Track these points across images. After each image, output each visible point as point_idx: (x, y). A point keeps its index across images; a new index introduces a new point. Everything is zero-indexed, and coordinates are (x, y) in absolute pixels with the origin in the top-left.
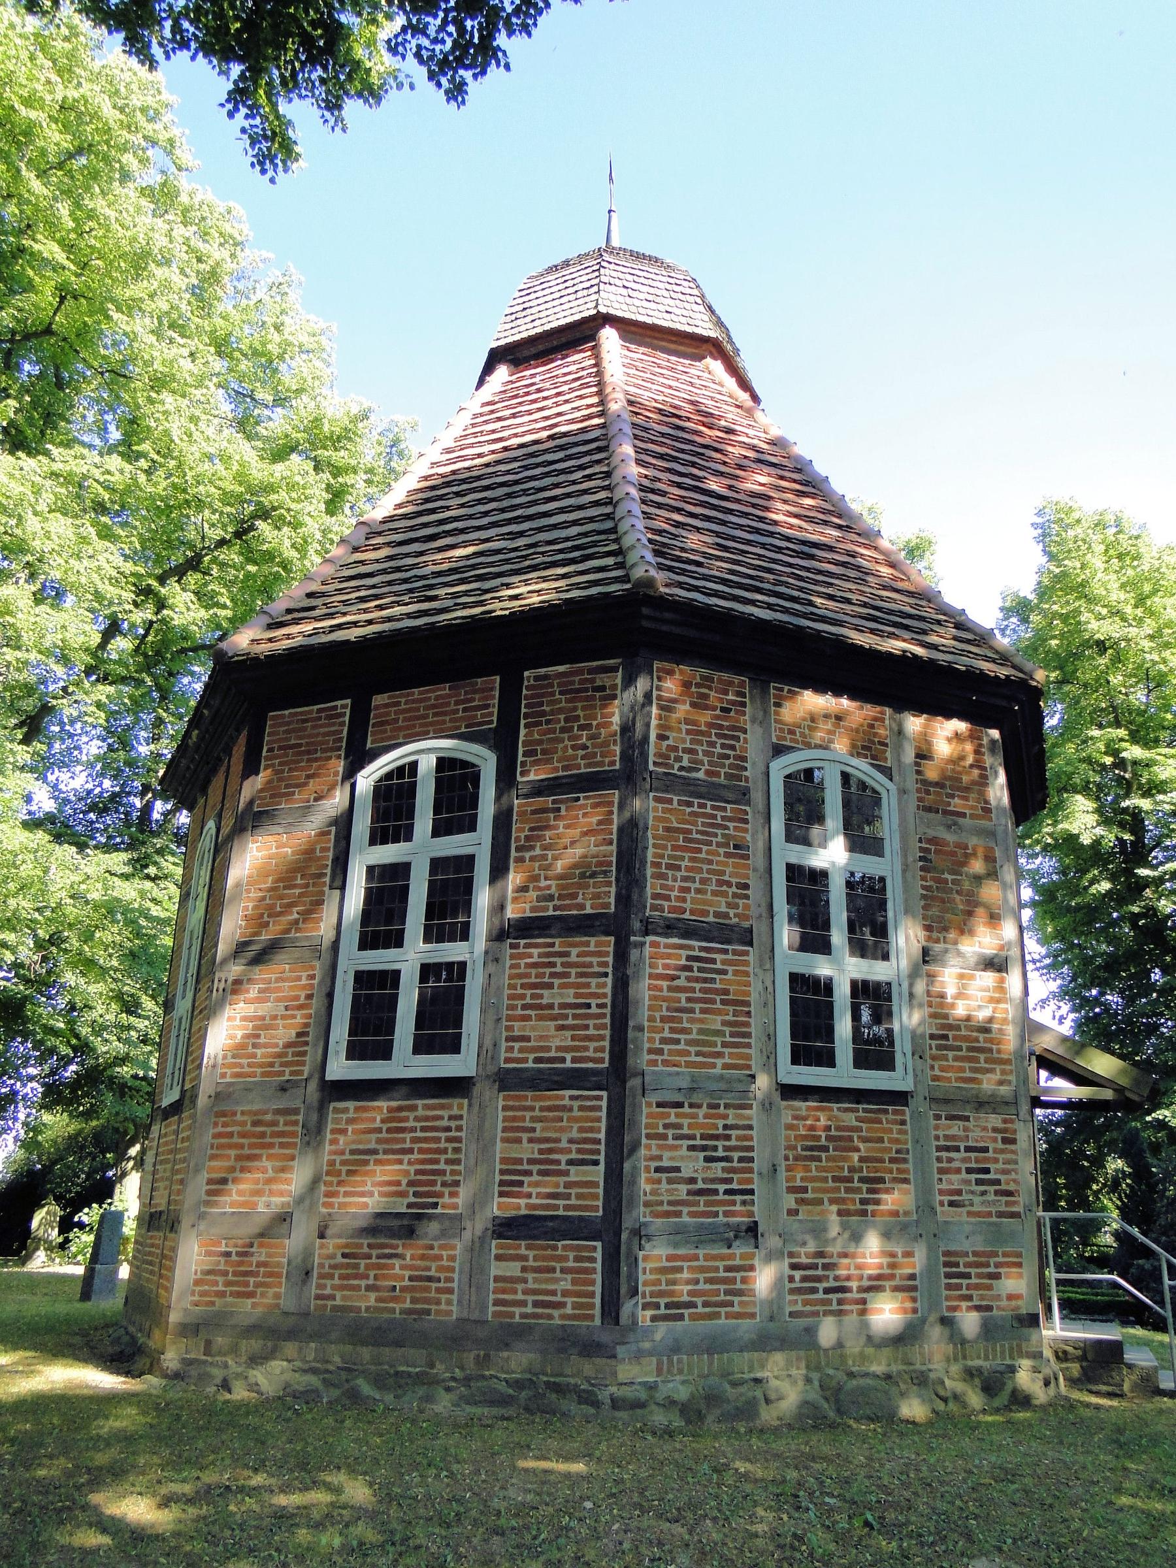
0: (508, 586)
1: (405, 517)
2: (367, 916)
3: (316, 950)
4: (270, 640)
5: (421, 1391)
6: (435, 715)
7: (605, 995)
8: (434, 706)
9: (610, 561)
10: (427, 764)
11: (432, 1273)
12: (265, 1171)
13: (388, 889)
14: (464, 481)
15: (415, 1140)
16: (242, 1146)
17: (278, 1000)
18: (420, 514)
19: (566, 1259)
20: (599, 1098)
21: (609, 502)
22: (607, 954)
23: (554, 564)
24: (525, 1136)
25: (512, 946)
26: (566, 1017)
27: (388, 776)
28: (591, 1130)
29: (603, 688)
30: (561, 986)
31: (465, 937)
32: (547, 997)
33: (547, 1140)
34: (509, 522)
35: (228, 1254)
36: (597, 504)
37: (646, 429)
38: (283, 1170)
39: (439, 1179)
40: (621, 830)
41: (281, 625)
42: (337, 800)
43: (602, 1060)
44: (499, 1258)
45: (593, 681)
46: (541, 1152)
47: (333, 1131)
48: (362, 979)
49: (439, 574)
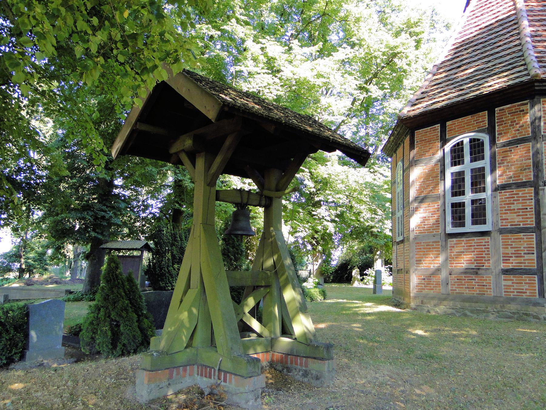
0: (487, 82)
1: (448, 60)
2: (452, 187)
3: (438, 197)
4: (413, 110)
5: (484, 314)
6: (467, 126)
7: (532, 205)
8: (466, 123)
9: (522, 68)
10: (466, 141)
11: (484, 284)
12: (432, 258)
13: (458, 180)
14: (467, 44)
15: (475, 249)
16: (424, 252)
17: (429, 212)
18: (454, 59)
19: (526, 280)
20: (533, 235)
21: (520, 44)
22: (532, 193)
23: (502, 72)
24: (509, 247)
25: (500, 193)
26: (519, 212)
27: (454, 146)
28: (531, 244)
29: (523, 111)
30: (517, 203)
31: (484, 191)
32: (512, 207)
33: (517, 248)
34: (485, 57)
35: (424, 279)
36: (516, 46)
37: (532, 11)
38: (437, 257)
39: (484, 259)
40: (533, 155)
41: (415, 105)
42: (440, 154)
43: (533, 224)
44: (504, 280)
45: (520, 108)
46: (515, 251)
47: (450, 247)
48: (453, 205)
49: (463, 80)
